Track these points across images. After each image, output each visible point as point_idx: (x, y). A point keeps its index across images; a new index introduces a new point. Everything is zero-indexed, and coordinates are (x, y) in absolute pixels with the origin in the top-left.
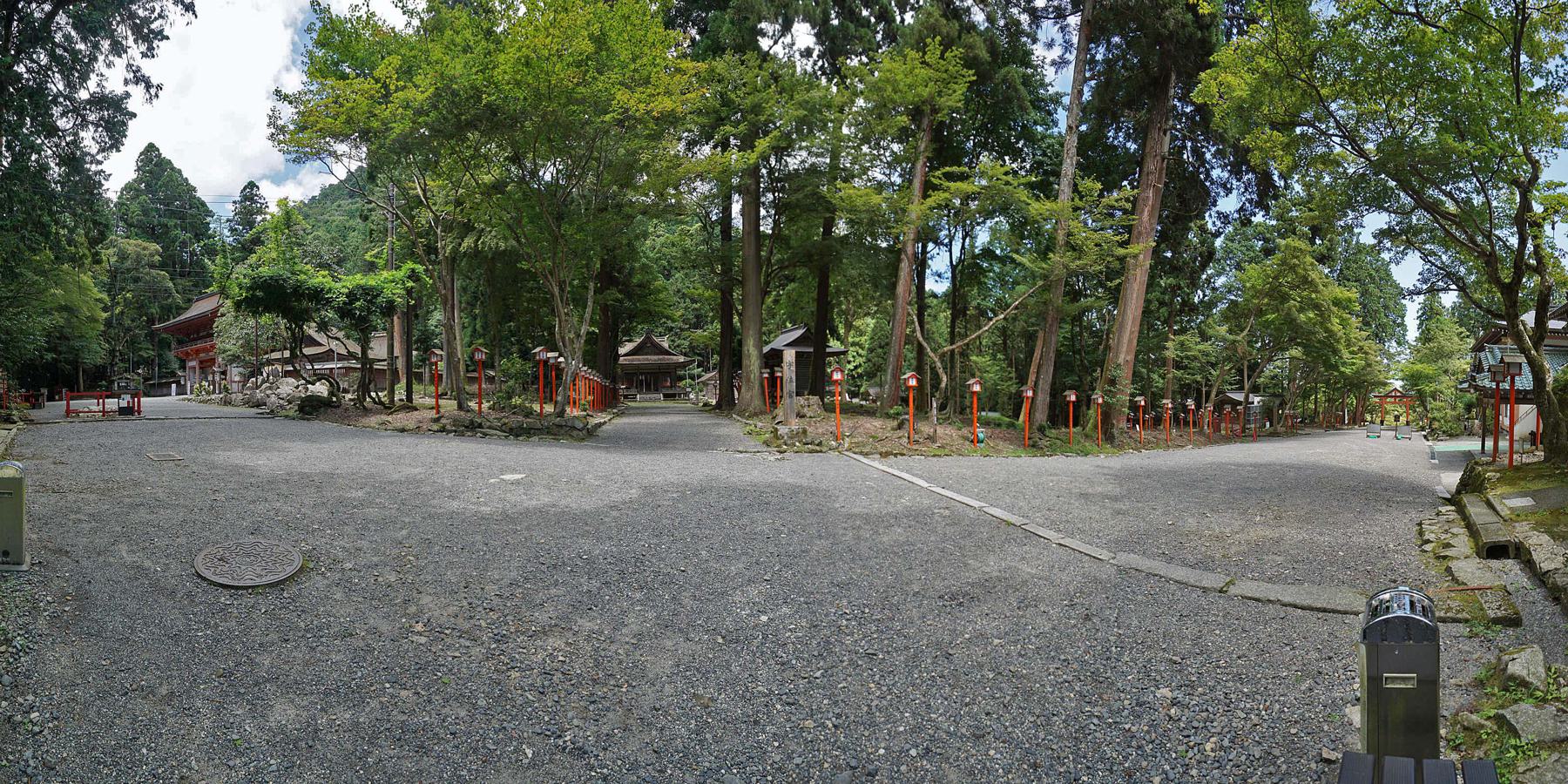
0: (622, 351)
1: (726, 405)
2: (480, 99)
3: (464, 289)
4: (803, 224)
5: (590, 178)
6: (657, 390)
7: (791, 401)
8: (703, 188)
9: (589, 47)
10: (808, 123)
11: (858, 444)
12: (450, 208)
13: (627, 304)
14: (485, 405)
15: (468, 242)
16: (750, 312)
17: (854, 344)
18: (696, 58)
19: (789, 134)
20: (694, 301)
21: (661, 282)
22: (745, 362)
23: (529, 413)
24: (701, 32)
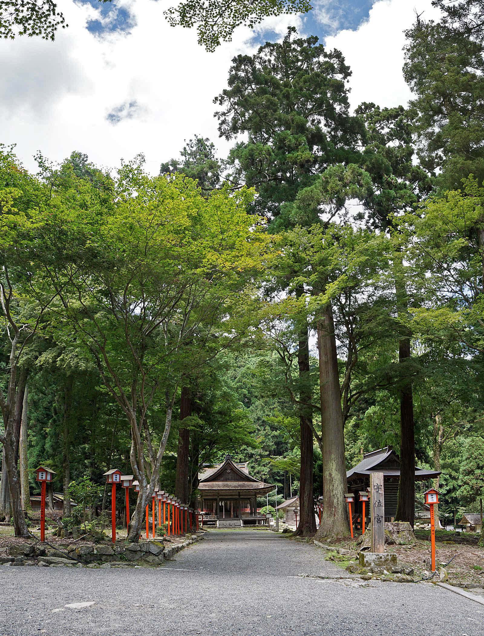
0: (202, 476)
1: (307, 530)
2: (84, 243)
3: (35, 404)
4: (378, 349)
5: (178, 316)
6: (237, 517)
7: (379, 526)
8: (281, 325)
9: (187, 222)
10: (369, 268)
11: (456, 576)
12: (32, 322)
13: (208, 430)
14: (50, 531)
15: (46, 357)
16: (331, 436)
17: (444, 467)
18: (272, 231)
19: (354, 277)
20: (273, 428)
21: (241, 410)
22: (326, 487)
23: (100, 539)
24: (275, 214)
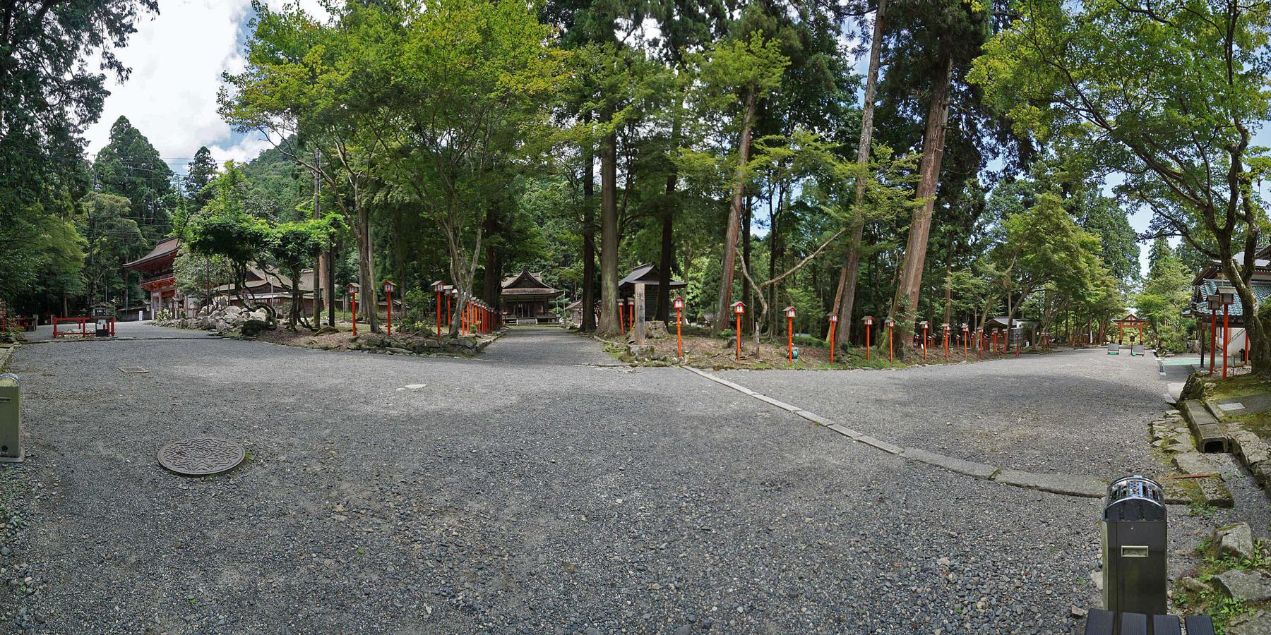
0: (504, 284)
1: (588, 328)
2: (389, 80)
3: (376, 234)
4: (651, 181)
5: (479, 144)
6: (532, 316)
7: (641, 325)
8: (570, 152)
9: (477, 38)
10: (655, 100)
11: (695, 360)
12: (365, 169)
13: (508, 246)
14: (393, 328)
15: (379, 196)
16: (608, 252)
17: (692, 279)
18: (564, 47)
19: (640, 109)
20: (562, 244)
21: (535, 228)
22: (604, 293)
23: (429, 335)
24: (568, 26)
